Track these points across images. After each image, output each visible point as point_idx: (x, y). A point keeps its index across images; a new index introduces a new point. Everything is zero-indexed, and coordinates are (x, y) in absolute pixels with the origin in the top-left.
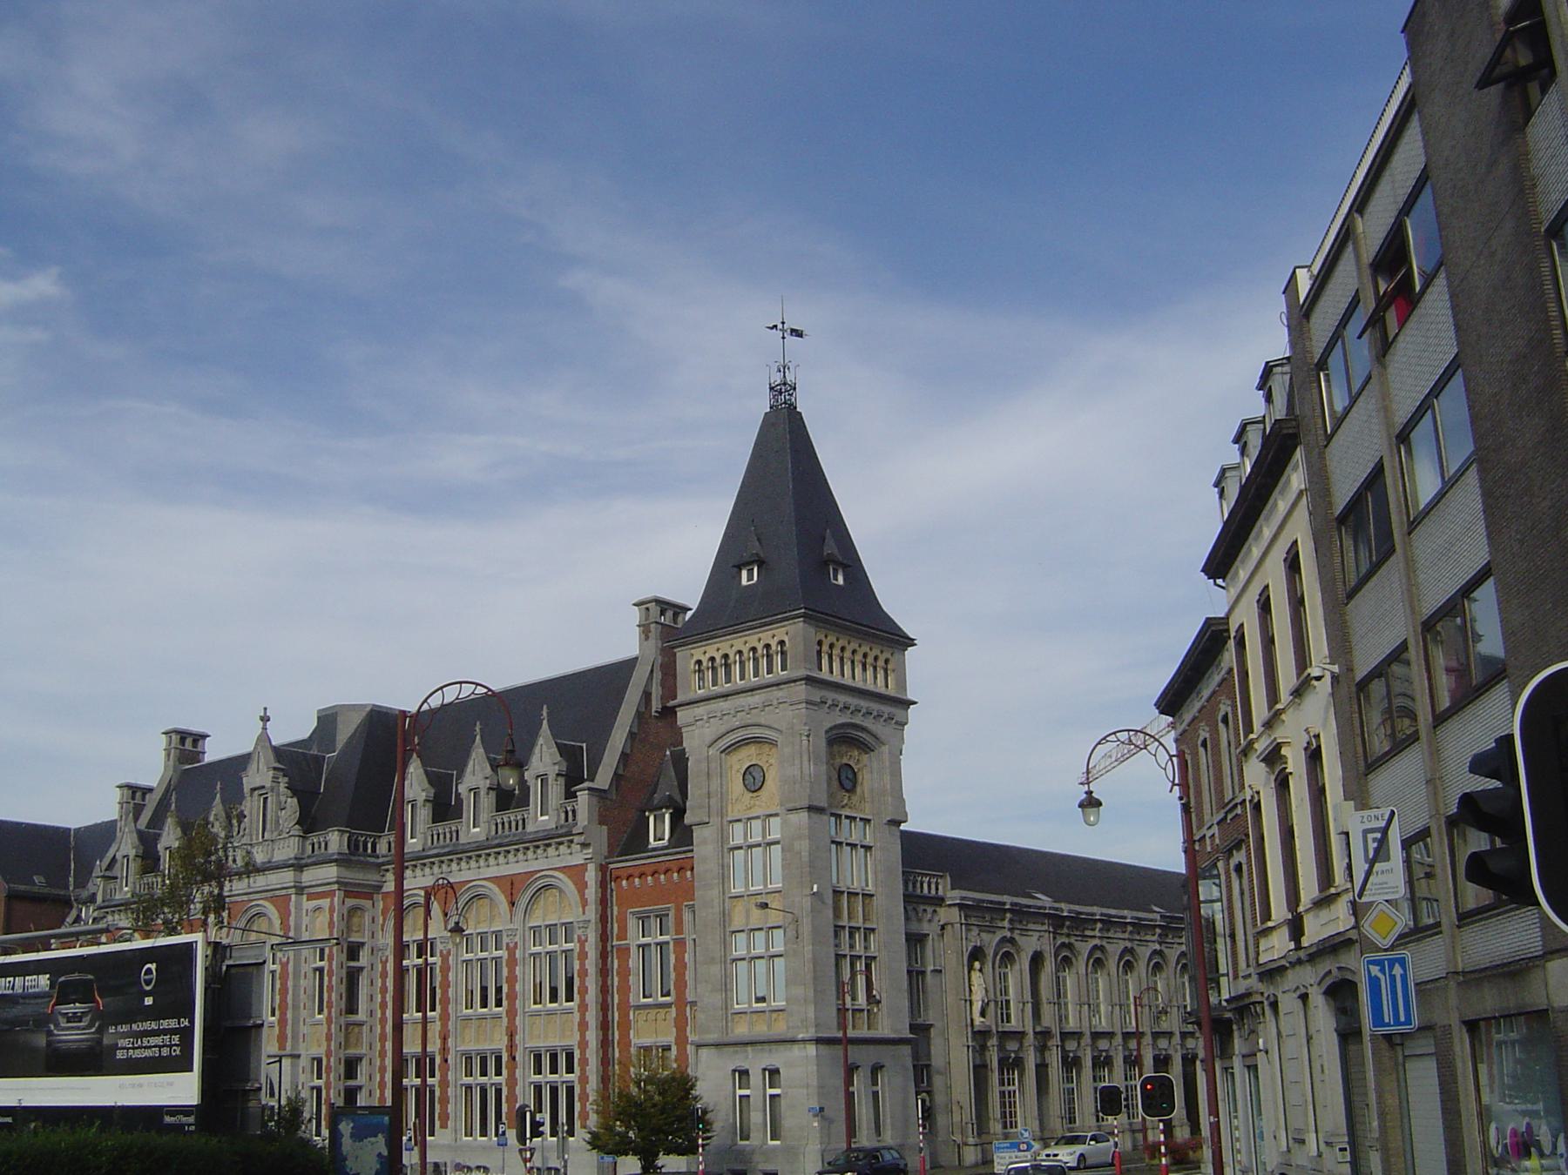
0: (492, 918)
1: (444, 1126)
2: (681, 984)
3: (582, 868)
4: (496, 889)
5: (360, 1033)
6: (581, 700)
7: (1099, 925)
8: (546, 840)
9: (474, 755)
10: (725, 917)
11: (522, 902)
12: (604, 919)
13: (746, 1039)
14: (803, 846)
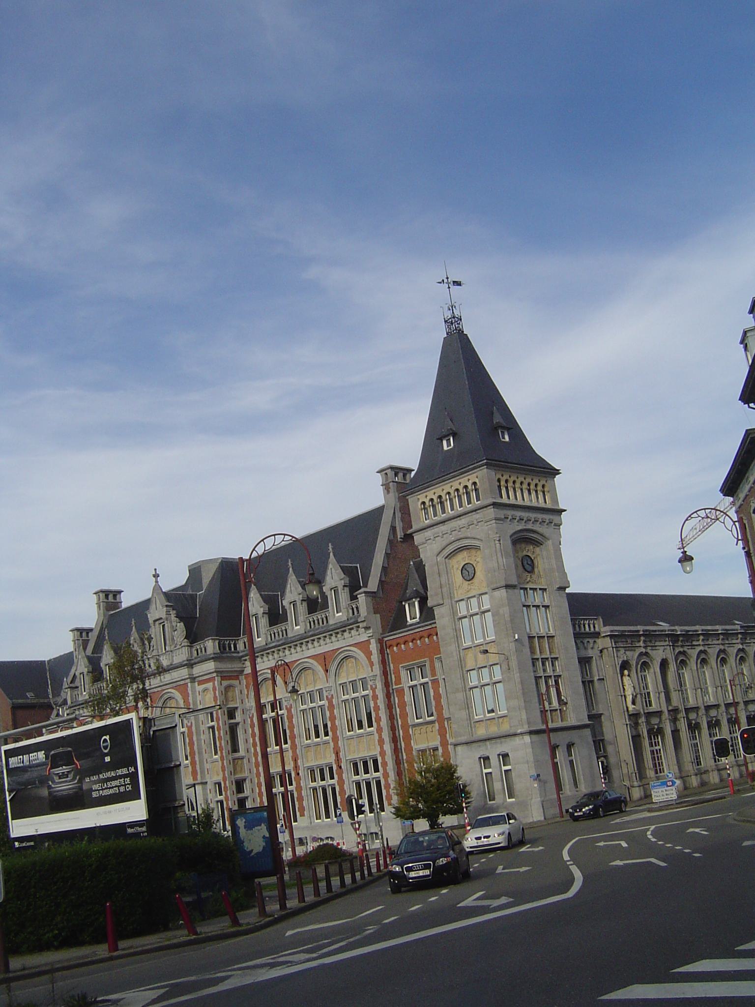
0: (315, 681)
1: (302, 815)
3: (368, 642)
4: (315, 663)
5: (242, 763)
6: (351, 538)
8: (343, 628)
9: (290, 581)
10: (461, 662)
12: (385, 673)
14: (505, 611)
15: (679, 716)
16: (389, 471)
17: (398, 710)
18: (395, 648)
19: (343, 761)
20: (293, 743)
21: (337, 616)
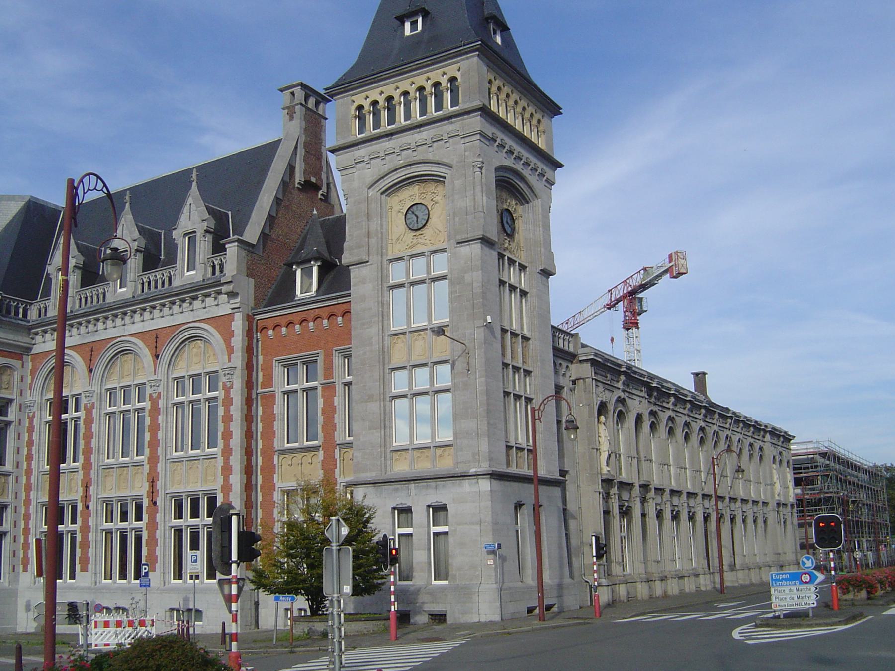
0: (135, 373)
1: (84, 569)
2: (330, 427)
3: (230, 316)
5: (6, 482)
6: (229, 181)
7: (672, 399)
8: (193, 292)
9: (123, 221)
10: (384, 354)
11: (166, 354)
12: (249, 367)
13: (409, 476)
14: (475, 278)
15: (648, 496)
16: (298, 91)
17: (260, 425)
18: (271, 332)
19: (161, 494)
20: (87, 460)
21: (185, 275)
